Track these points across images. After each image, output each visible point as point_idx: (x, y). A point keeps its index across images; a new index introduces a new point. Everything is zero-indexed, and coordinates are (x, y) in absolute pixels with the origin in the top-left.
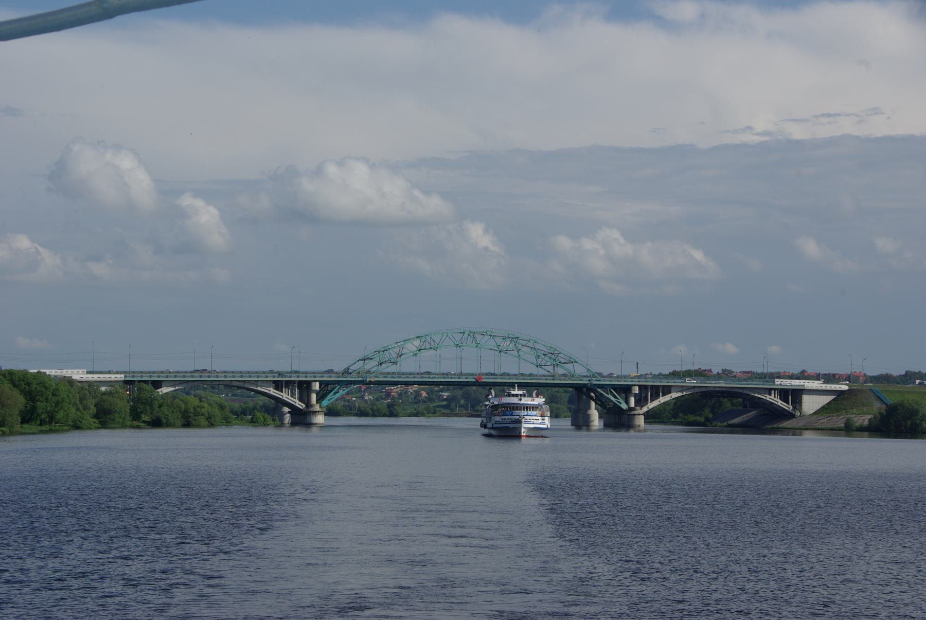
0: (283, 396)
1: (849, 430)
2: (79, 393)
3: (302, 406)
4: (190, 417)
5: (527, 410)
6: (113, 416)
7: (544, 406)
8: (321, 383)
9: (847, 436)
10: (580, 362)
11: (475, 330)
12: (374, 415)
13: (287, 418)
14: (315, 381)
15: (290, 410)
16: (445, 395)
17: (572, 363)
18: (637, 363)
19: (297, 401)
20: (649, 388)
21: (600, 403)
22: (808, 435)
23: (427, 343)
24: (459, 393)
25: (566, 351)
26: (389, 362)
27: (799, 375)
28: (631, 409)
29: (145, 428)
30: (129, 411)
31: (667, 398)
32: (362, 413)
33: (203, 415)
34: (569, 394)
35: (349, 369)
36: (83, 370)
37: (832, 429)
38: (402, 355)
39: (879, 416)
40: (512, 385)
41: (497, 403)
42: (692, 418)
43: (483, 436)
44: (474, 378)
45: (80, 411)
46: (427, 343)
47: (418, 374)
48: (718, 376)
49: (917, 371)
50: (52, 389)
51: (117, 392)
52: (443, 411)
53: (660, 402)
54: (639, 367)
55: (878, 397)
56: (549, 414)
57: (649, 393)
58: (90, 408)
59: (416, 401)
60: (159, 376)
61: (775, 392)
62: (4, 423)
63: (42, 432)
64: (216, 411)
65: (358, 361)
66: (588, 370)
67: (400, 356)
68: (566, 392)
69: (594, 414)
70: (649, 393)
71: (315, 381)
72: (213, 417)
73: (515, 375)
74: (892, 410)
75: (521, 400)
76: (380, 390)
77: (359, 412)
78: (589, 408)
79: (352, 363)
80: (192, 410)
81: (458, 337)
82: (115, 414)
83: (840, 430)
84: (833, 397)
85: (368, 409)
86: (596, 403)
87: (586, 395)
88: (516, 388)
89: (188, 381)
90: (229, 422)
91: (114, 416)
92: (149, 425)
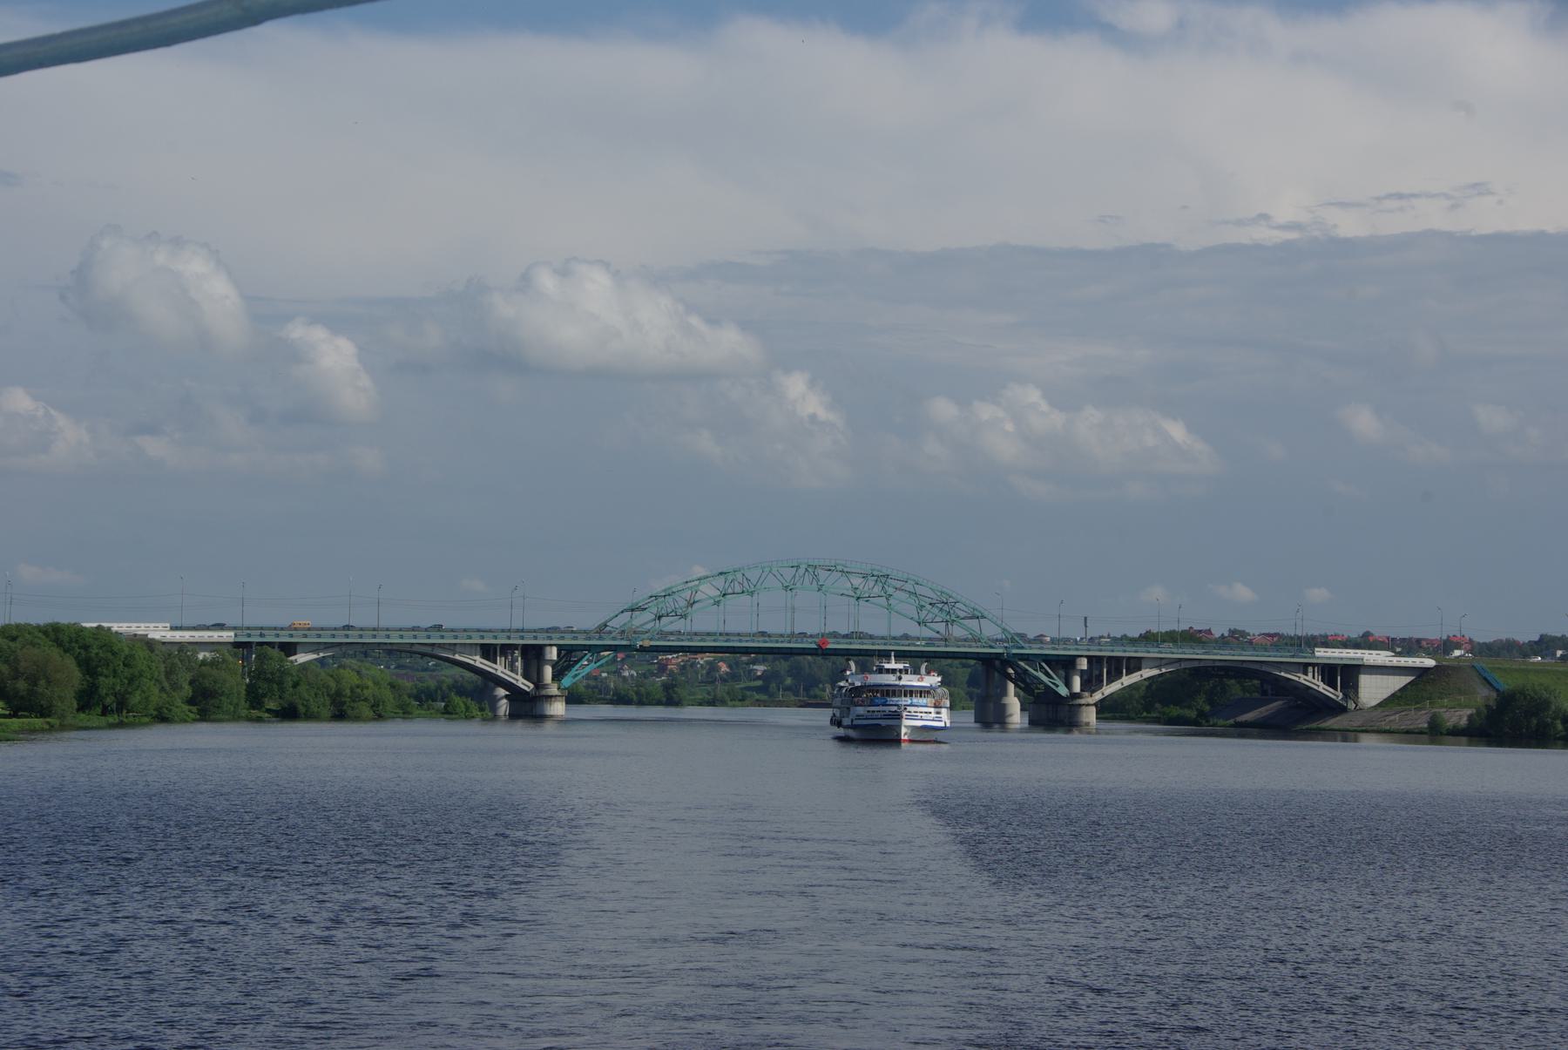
0: (496, 670)
1: (1436, 733)
2: (164, 662)
3: (529, 687)
4: (345, 702)
5: (911, 696)
6: (218, 701)
7: (939, 690)
8: (560, 648)
9: (1432, 742)
10: (990, 616)
11: (816, 563)
12: (641, 703)
13: (503, 707)
14: (551, 645)
15: (507, 693)
16: (760, 669)
17: (978, 618)
18: (1086, 618)
19: (519, 677)
20: (1105, 660)
21: (1023, 685)
22: (1367, 740)
23: (736, 583)
24: (783, 665)
25: (958, 594)
26: (673, 614)
27: (1359, 640)
28: (1075, 696)
29: (269, 722)
30: (244, 692)
31: (1134, 678)
32: (620, 699)
33: (366, 700)
34: (969, 670)
35: (606, 626)
36: (164, 625)
37: (1408, 732)
38: (694, 603)
39: (1486, 711)
40: (885, 655)
41: (860, 684)
42: (1175, 711)
43: (836, 743)
44: (815, 643)
45: (167, 693)
46: (736, 583)
47: (721, 634)
48: (1223, 642)
49: (1559, 635)
50: (123, 656)
51: (224, 661)
52: (757, 697)
53: (1122, 684)
54: (1088, 625)
55: (1485, 679)
56: (948, 703)
57: (1105, 670)
58: (181, 688)
59: (710, 680)
60: (291, 636)
61: (1314, 671)
62: (50, 711)
63: (112, 726)
64: (388, 694)
65: (622, 612)
66: (1004, 630)
67: (692, 605)
68: (964, 666)
69: (1013, 703)
70: (1105, 670)
71: (551, 645)
72: (381, 703)
73: (883, 638)
74: (1506, 701)
75: (900, 678)
76: (648, 661)
77: (615, 698)
78: (1004, 693)
79: (612, 615)
80: (348, 692)
81: (790, 572)
82: (223, 698)
83: (1421, 733)
84: (1410, 679)
85: (631, 692)
86: (1016, 686)
87: (999, 672)
88: (893, 658)
89: (340, 644)
90: (409, 713)
91: (221, 700)
92: (277, 717)
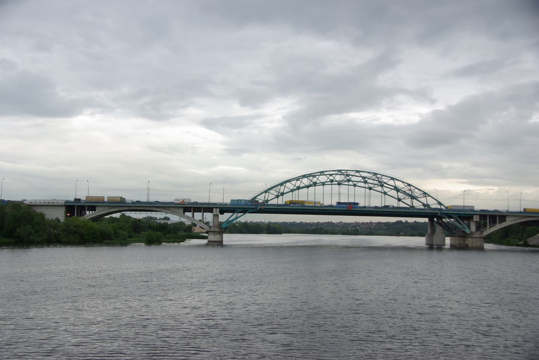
31: (504, 225)
